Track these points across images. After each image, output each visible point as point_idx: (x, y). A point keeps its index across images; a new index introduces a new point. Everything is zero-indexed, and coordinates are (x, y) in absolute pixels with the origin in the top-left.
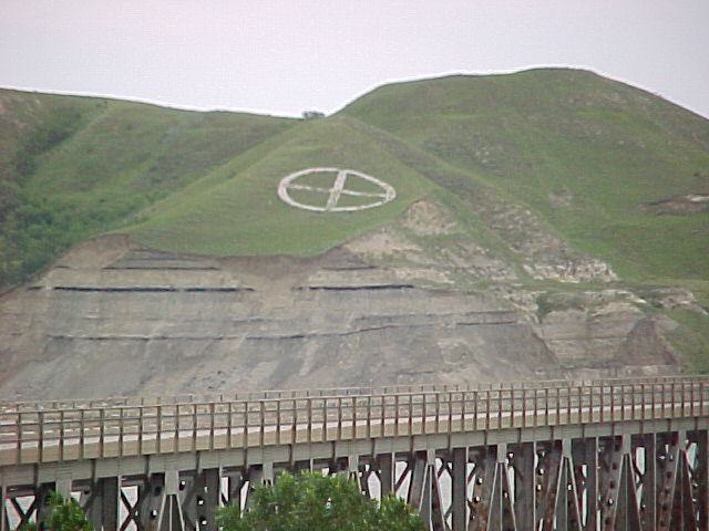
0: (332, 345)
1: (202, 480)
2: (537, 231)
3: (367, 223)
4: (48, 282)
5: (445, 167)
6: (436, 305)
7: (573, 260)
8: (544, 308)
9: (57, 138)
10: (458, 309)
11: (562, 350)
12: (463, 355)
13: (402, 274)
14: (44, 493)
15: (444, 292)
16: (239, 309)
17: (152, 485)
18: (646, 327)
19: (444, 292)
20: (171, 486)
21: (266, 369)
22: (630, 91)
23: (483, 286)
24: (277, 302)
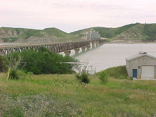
0: (43, 40)
1: (37, 47)
2: (97, 93)
3: (45, 35)
4: (30, 37)
5: (49, 32)
6: (48, 38)
7: (54, 36)
8: (53, 38)
9: (30, 31)
10: (49, 39)
11: (54, 40)
12: (49, 41)
13: (46, 37)
14: (30, 47)
15: (48, 38)
16: (39, 39)
17: (35, 47)
18: (58, 39)
19: (48, 38)
20: (36, 47)
21: (40, 41)
22: (10, 28)
23: (50, 38)
24: (41, 38)
